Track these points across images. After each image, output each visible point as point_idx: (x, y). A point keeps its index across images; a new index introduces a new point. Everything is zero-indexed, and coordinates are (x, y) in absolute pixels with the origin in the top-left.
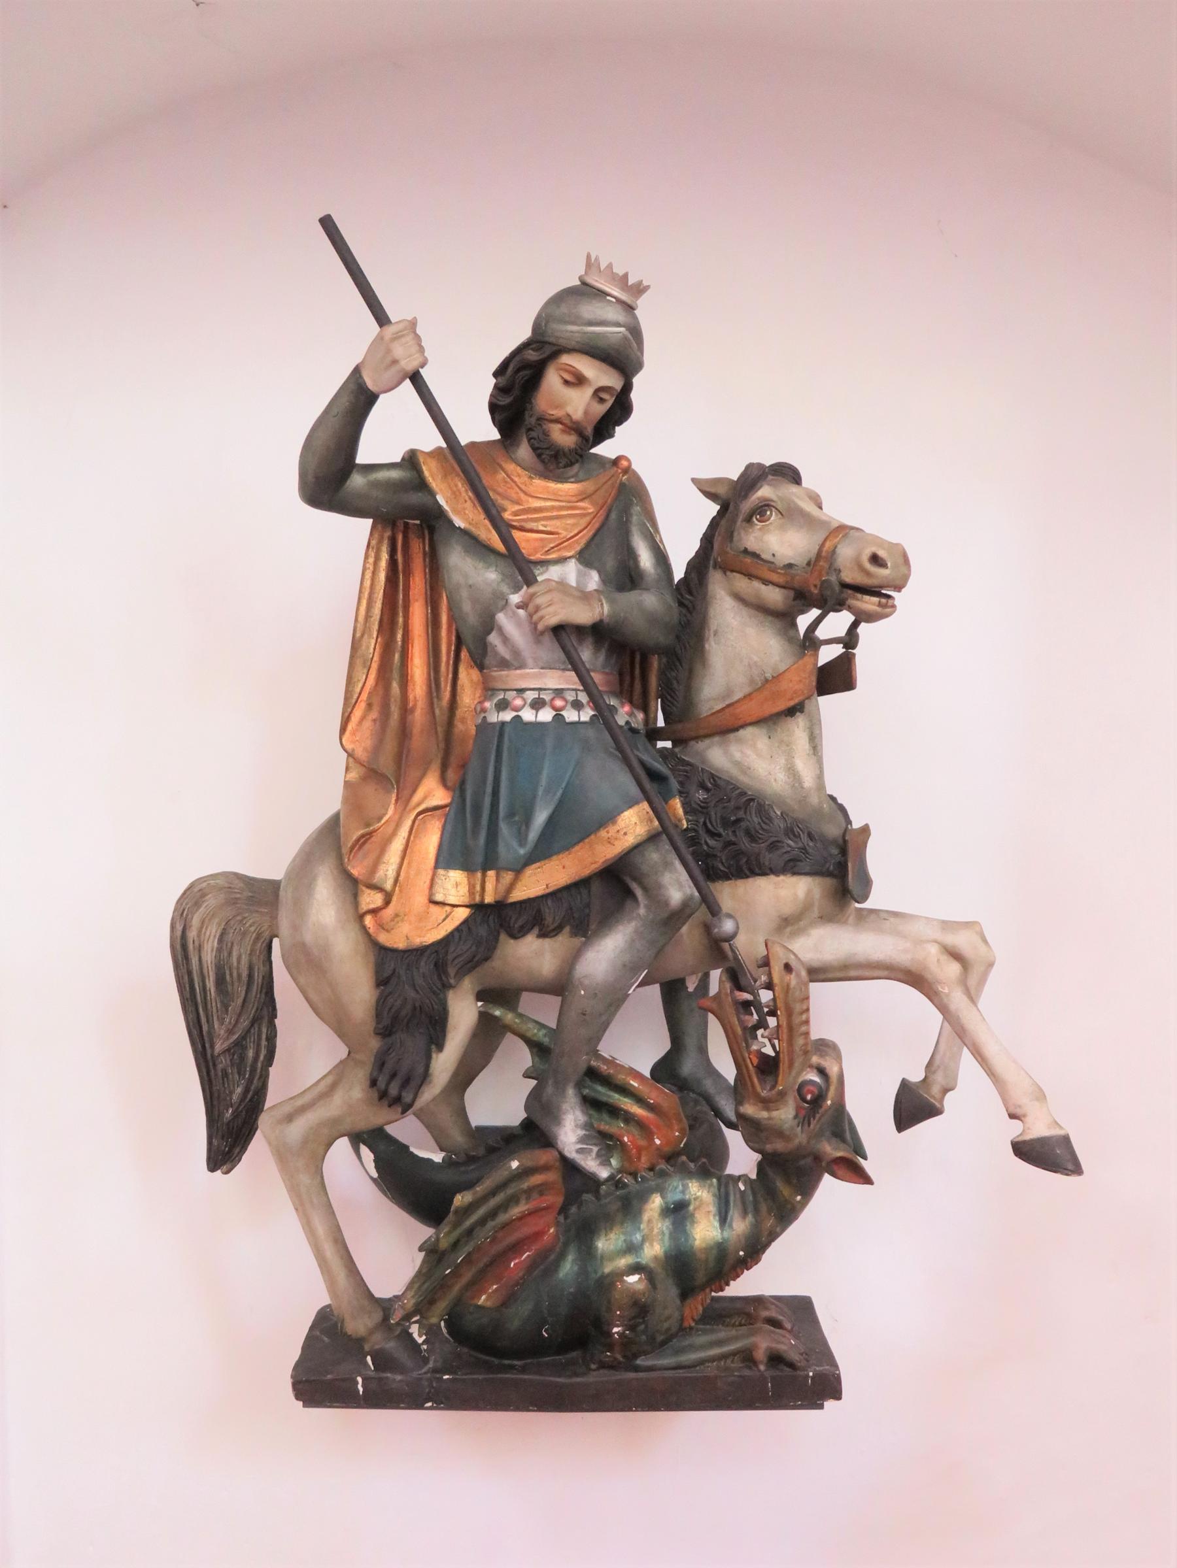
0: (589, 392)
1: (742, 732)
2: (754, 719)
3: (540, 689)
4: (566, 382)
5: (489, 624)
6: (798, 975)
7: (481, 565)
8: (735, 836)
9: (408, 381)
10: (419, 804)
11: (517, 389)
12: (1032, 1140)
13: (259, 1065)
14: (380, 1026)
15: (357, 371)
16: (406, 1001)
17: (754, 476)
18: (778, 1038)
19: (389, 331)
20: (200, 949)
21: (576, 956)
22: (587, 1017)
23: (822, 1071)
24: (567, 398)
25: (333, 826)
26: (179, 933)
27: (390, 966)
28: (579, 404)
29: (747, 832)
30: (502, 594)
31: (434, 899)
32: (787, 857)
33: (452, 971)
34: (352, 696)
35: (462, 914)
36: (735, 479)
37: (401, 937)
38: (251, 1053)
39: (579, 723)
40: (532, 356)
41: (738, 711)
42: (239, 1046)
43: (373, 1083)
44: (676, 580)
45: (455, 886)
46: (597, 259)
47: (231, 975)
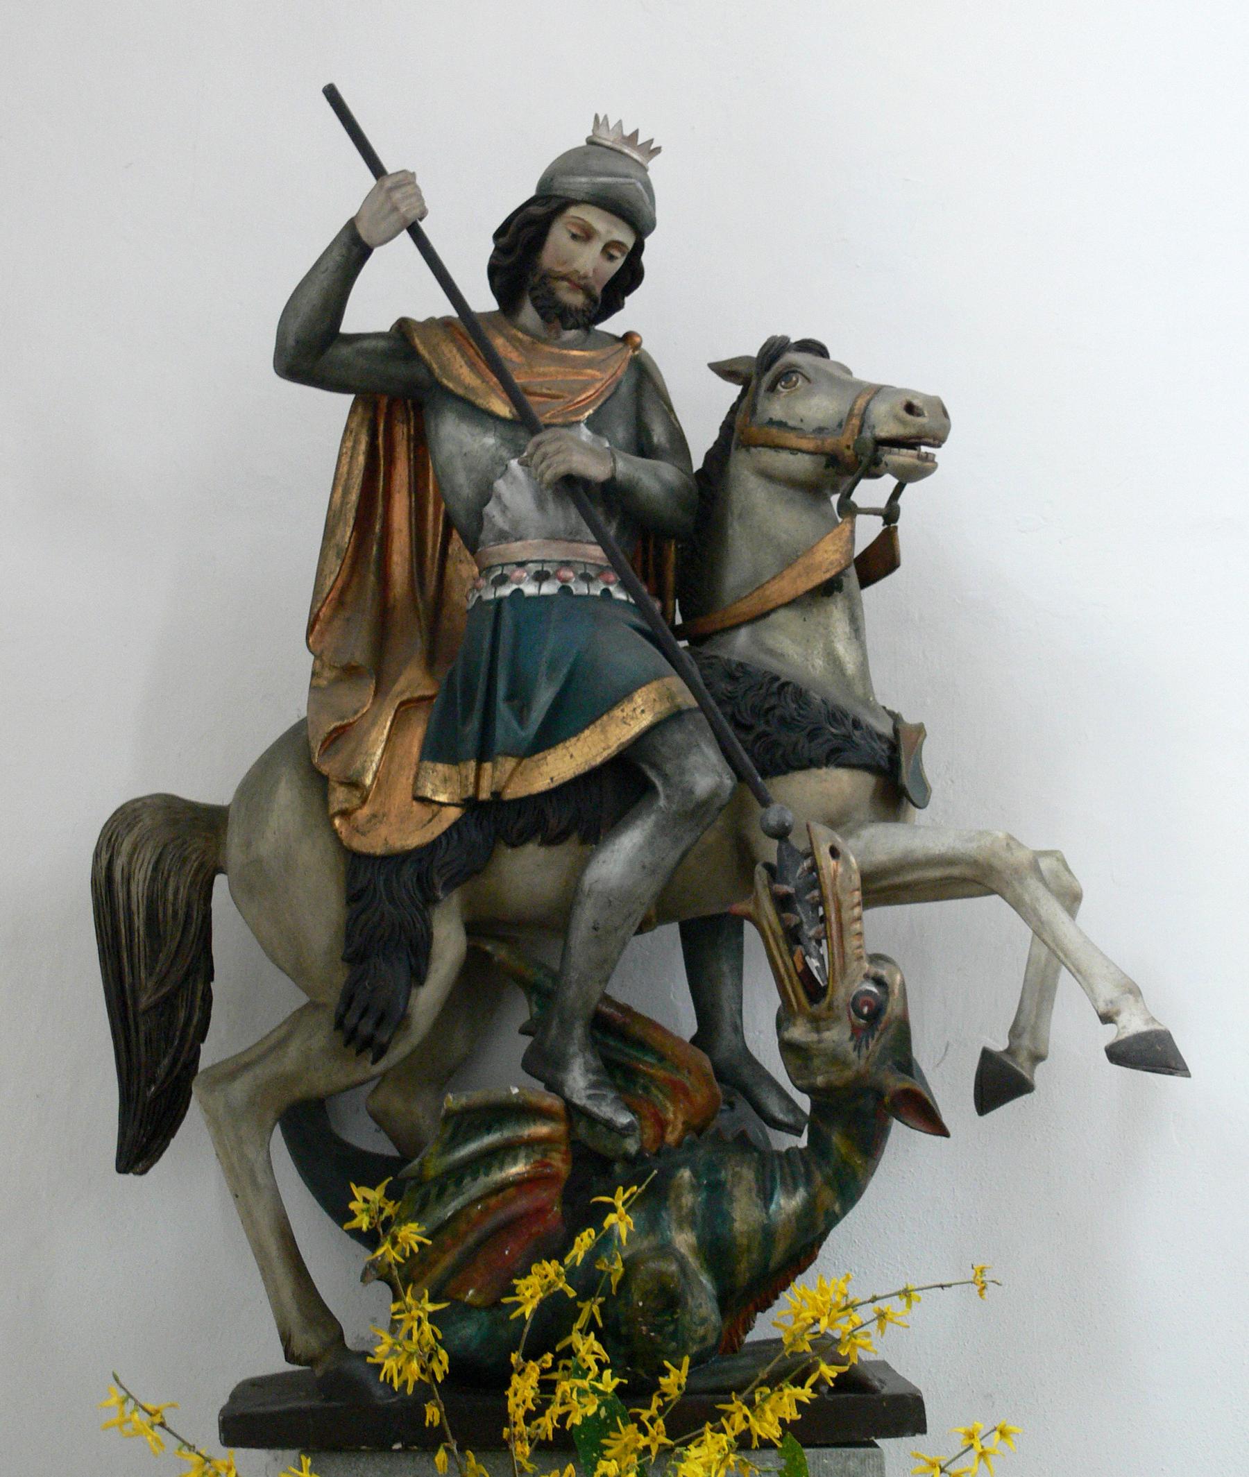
0: (596, 247)
1: (773, 617)
2: (786, 599)
3: (543, 562)
4: (574, 237)
5: (486, 493)
6: (847, 862)
7: (478, 430)
8: (781, 728)
9: (405, 232)
10: (402, 692)
11: (520, 246)
12: (1128, 1038)
13: (192, 1030)
14: (350, 950)
15: (351, 225)
16: (382, 903)
17: (775, 350)
18: (826, 937)
19: (388, 183)
20: (128, 880)
21: (583, 864)
22: (599, 932)
23: (879, 981)
24: (577, 255)
25: (296, 737)
26: (104, 863)
27: (364, 876)
28: (590, 262)
29: (782, 720)
30: (501, 458)
31: (410, 798)
32: (826, 747)
33: (438, 882)
34: (323, 590)
35: (453, 814)
36: (755, 354)
37: (375, 842)
38: (182, 1014)
39: (588, 596)
40: (536, 210)
41: (768, 593)
42: (167, 1005)
43: (339, 1024)
44: (695, 470)
45: (444, 786)
46: (606, 118)
47: (165, 909)
